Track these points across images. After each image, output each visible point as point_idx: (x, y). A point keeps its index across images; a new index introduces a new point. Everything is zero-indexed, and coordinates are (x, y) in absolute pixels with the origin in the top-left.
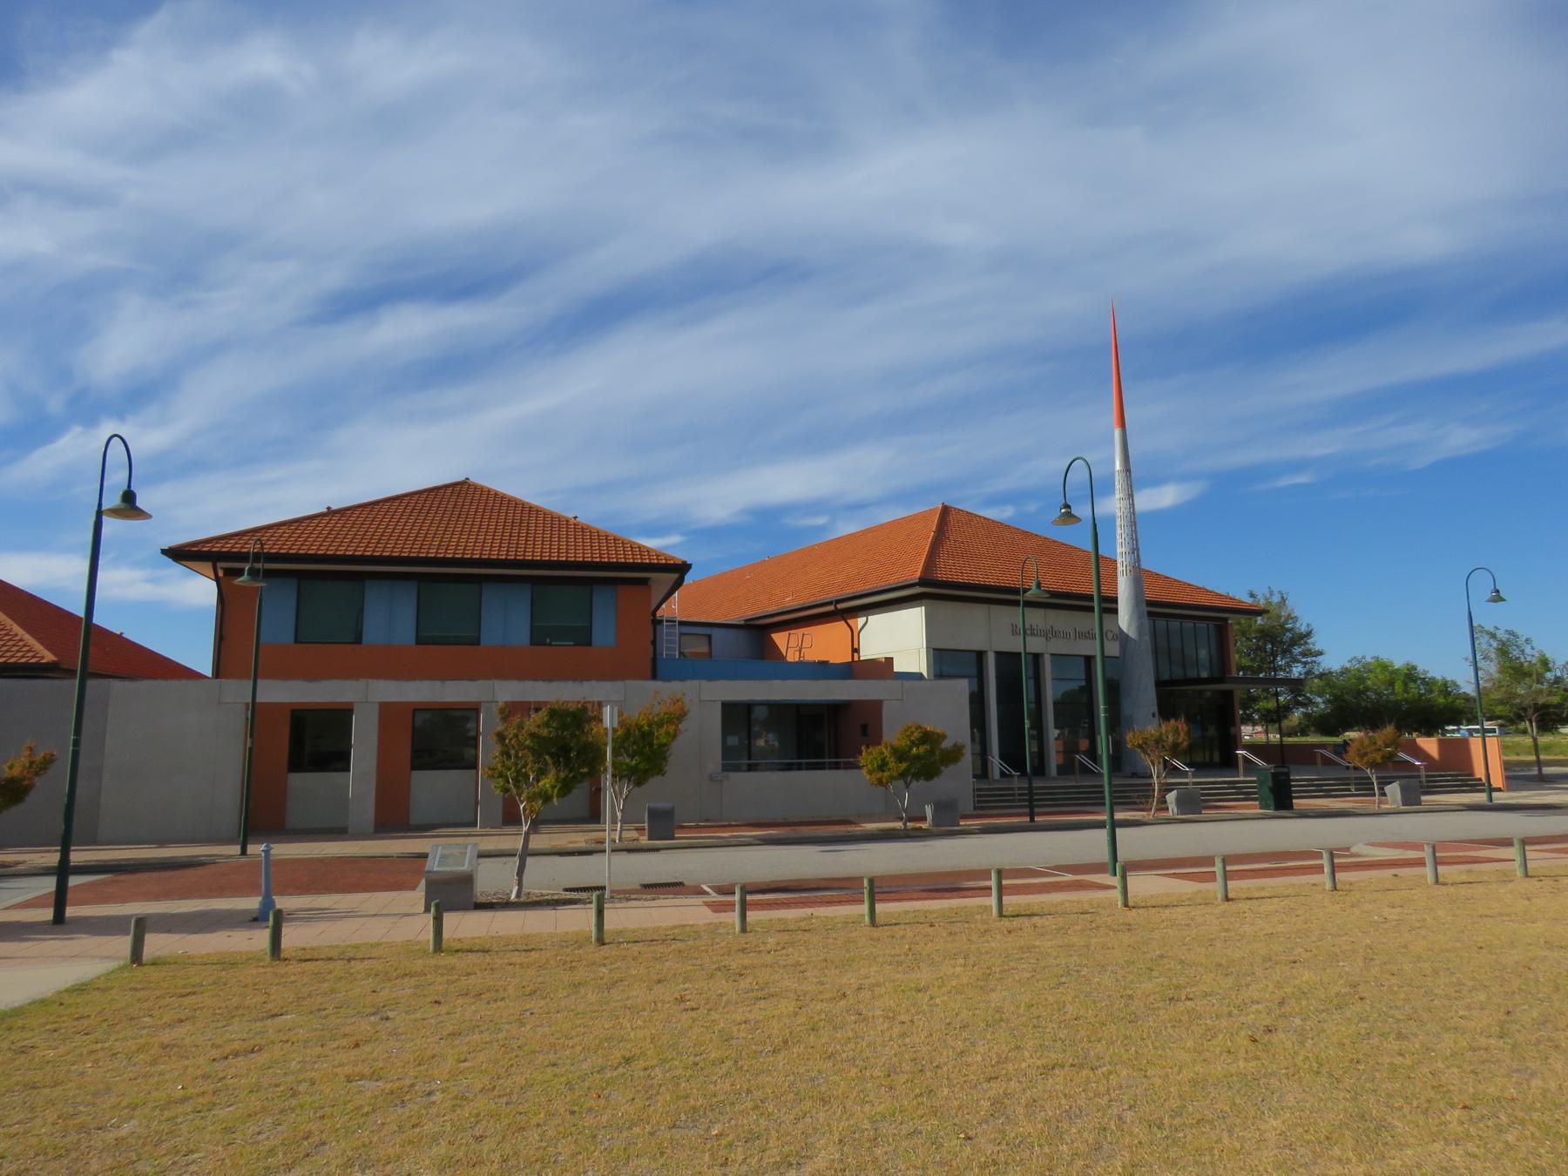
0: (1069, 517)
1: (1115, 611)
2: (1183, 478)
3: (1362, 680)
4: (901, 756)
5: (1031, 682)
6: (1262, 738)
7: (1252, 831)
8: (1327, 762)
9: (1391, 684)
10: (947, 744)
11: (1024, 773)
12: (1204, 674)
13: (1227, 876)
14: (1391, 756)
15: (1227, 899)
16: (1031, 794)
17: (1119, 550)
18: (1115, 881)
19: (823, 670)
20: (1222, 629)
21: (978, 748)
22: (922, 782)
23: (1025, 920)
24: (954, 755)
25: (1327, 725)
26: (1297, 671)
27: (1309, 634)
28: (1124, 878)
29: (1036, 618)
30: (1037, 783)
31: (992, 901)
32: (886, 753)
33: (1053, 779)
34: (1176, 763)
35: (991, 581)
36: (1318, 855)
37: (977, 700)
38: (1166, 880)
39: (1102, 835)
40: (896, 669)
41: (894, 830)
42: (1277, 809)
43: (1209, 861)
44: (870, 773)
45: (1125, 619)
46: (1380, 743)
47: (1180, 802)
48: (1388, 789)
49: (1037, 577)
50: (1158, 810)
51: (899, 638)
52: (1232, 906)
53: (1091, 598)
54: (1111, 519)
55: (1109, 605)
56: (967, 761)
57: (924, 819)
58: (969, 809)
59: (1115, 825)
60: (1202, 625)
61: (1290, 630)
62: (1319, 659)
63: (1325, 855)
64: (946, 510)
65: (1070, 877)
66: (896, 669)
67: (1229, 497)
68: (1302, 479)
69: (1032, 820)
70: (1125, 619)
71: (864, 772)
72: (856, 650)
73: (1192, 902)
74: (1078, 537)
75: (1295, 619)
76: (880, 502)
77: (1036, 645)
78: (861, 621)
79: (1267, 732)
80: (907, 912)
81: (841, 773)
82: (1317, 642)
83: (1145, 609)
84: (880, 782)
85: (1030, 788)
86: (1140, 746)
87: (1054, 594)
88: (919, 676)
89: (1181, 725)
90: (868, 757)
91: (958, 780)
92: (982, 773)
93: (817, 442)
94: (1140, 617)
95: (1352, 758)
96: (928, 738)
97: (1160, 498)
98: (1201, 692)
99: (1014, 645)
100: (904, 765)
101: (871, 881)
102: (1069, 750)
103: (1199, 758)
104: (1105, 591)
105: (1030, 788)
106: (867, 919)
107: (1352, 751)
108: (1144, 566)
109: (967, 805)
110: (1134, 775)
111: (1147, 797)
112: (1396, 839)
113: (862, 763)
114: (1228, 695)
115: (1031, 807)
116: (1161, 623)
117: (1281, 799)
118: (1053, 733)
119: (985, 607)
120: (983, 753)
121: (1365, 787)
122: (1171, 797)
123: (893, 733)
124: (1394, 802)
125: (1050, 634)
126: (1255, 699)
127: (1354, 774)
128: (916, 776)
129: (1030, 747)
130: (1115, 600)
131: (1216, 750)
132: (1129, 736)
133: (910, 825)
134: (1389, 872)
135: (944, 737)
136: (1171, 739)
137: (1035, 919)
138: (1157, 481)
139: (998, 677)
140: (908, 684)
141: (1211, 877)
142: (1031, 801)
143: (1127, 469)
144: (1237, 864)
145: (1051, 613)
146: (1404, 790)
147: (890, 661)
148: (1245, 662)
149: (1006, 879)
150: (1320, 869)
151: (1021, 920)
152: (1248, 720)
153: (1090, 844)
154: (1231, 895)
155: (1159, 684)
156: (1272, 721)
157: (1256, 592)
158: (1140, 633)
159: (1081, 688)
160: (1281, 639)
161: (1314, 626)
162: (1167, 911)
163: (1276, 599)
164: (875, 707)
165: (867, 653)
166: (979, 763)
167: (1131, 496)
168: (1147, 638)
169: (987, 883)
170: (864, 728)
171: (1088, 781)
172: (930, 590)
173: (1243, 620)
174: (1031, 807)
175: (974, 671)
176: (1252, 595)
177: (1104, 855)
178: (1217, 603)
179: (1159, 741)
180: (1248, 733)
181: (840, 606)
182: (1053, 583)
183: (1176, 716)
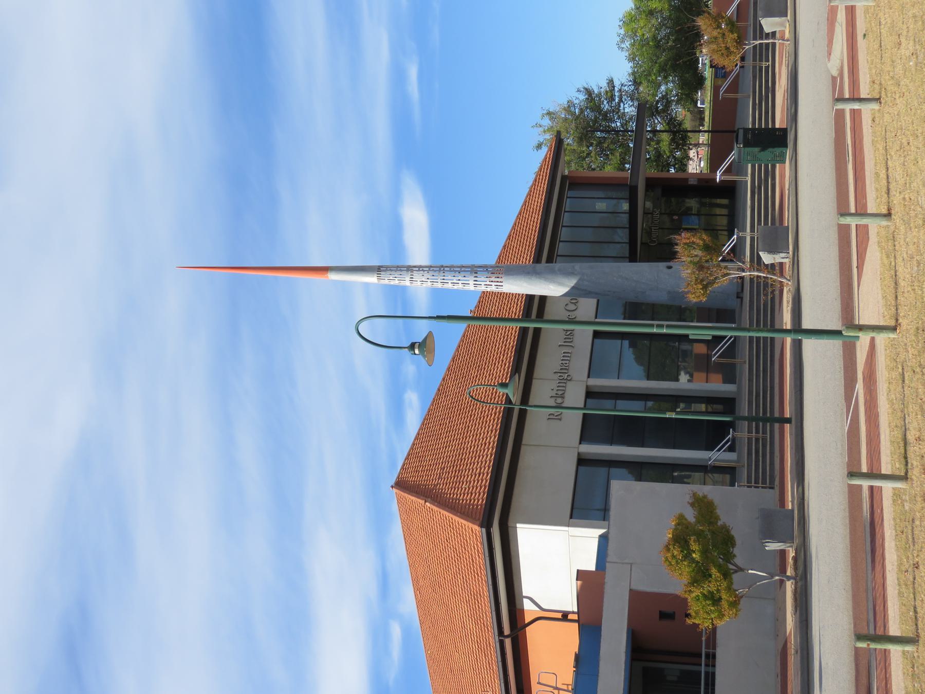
0: (423, 346)
1: (543, 299)
2: (396, 197)
3: (643, 43)
4: (701, 575)
5: (621, 403)
6: (704, 151)
7: (810, 177)
8: (734, 87)
9: (651, 13)
10: (690, 515)
11: (731, 425)
12: (625, 206)
13: (861, 212)
14: (730, 23)
15: (888, 215)
16: (757, 419)
17: (471, 287)
18: (864, 339)
19: (586, 662)
20: (574, 183)
21: (698, 475)
22: (736, 551)
23: (911, 450)
24: (705, 508)
25: (692, 82)
26: (629, 109)
27: (589, 92)
28: (861, 328)
29: (542, 391)
30: (744, 409)
31: (888, 487)
32: (697, 592)
33: (738, 388)
34: (726, 249)
35: (494, 439)
36: (840, 115)
37: (641, 470)
38: (864, 278)
39: (809, 344)
40: (592, 567)
41: (795, 593)
42: (785, 145)
43: (844, 231)
44: (721, 616)
45: (553, 288)
46: (715, 33)
47: (773, 249)
48: (767, 29)
49: (494, 384)
50: (782, 275)
51: (554, 560)
52: (897, 211)
53: (524, 331)
54: (436, 294)
55: (535, 306)
56: (712, 491)
57: (783, 553)
58: (773, 494)
59: (797, 329)
60: (568, 204)
61: (582, 111)
62: (617, 84)
63: (840, 106)
64: (401, 485)
65: (860, 387)
66: (592, 567)
67: (425, 149)
68: (413, 72)
69: (788, 421)
70: (553, 288)
71: (719, 623)
72: (565, 616)
73: (891, 253)
74: (449, 338)
75: (570, 104)
76: (382, 554)
77: (575, 395)
78: (528, 605)
79: (697, 145)
80: (900, 594)
81: (720, 653)
82: (598, 84)
83: (543, 265)
84: (734, 604)
85: (749, 419)
86: (705, 287)
87: (516, 369)
88: (603, 539)
89: (683, 239)
90: (701, 616)
91: (736, 505)
92: (729, 473)
93: (295, 624)
94: (553, 272)
95: (731, 63)
96: (681, 538)
97: (416, 219)
98: (646, 213)
99: (573, 421)
100: (714, 571)
101: (859, 637)
102: (704, 365)
103: (724, 221)
104: (517, 310)
105: (749, 419)
106: (909, 648)
107: (721, 61)
108: (492, 260)
109: (769, 497)
110: (739, 296)
111: (766, 285)
112: (824, 27)
113: (707, 624)
114: (651, 183)
115: (773, 420)
116: (562, 248)
117: (776, 140)
118: (683, 383)
119: (523, 449)
120: (703, 468)
121: (766, 52)
122: (767, 258)
123: (674, 581)
124: (783, 25)
125: (564, 375)
126: (659, 155)
127: (749, 62)
128: (729, 557)
129: (700, 414)
130: (530, 298)
131: (714, 202)
132: (693, 299)
133: (790, 572)
134: (861, 43)
135: (681, 517)
136: (698, 252)
137: (911, 437)
138: (395, 230)
139: (611, 442)
140: (611, 556)
141: (863, 231)
142: (765, 420)
143: (378, 270)
144: (848, 199)
145: (538, 372)
146: (770, 14)
147: (581, 575)
148: (616, 159)
149: (860, 468)
150: (855, 114)
151: (910, 455)
152: (682, 165)
153: (820, 361)
154: (885, 211)
155: (633, 258)
156: (685, 138)
157: (536, 143)
158: (569, 274)
159: (632, 345)
160: (591, 120)
161: (581, 84)
162: (902, 283)
163: (547, 122)
164: (636, 598)
165: (571, 605)
166: (717, 476)
167: (410, 269)
168: (577, 266)
169: (866, 493)
170: (664, 616)
171: (744, 353)
172: (497, 516)
173: (565, 158)
174: (773, 420)
175: (603, 471)
176: (539, 146)
177: (833, 346)
178: (544, 186)
179: (700, 267)
180: (697, 164)
181: (507, 631)
182: (502, 367)
183: (672, 244)
